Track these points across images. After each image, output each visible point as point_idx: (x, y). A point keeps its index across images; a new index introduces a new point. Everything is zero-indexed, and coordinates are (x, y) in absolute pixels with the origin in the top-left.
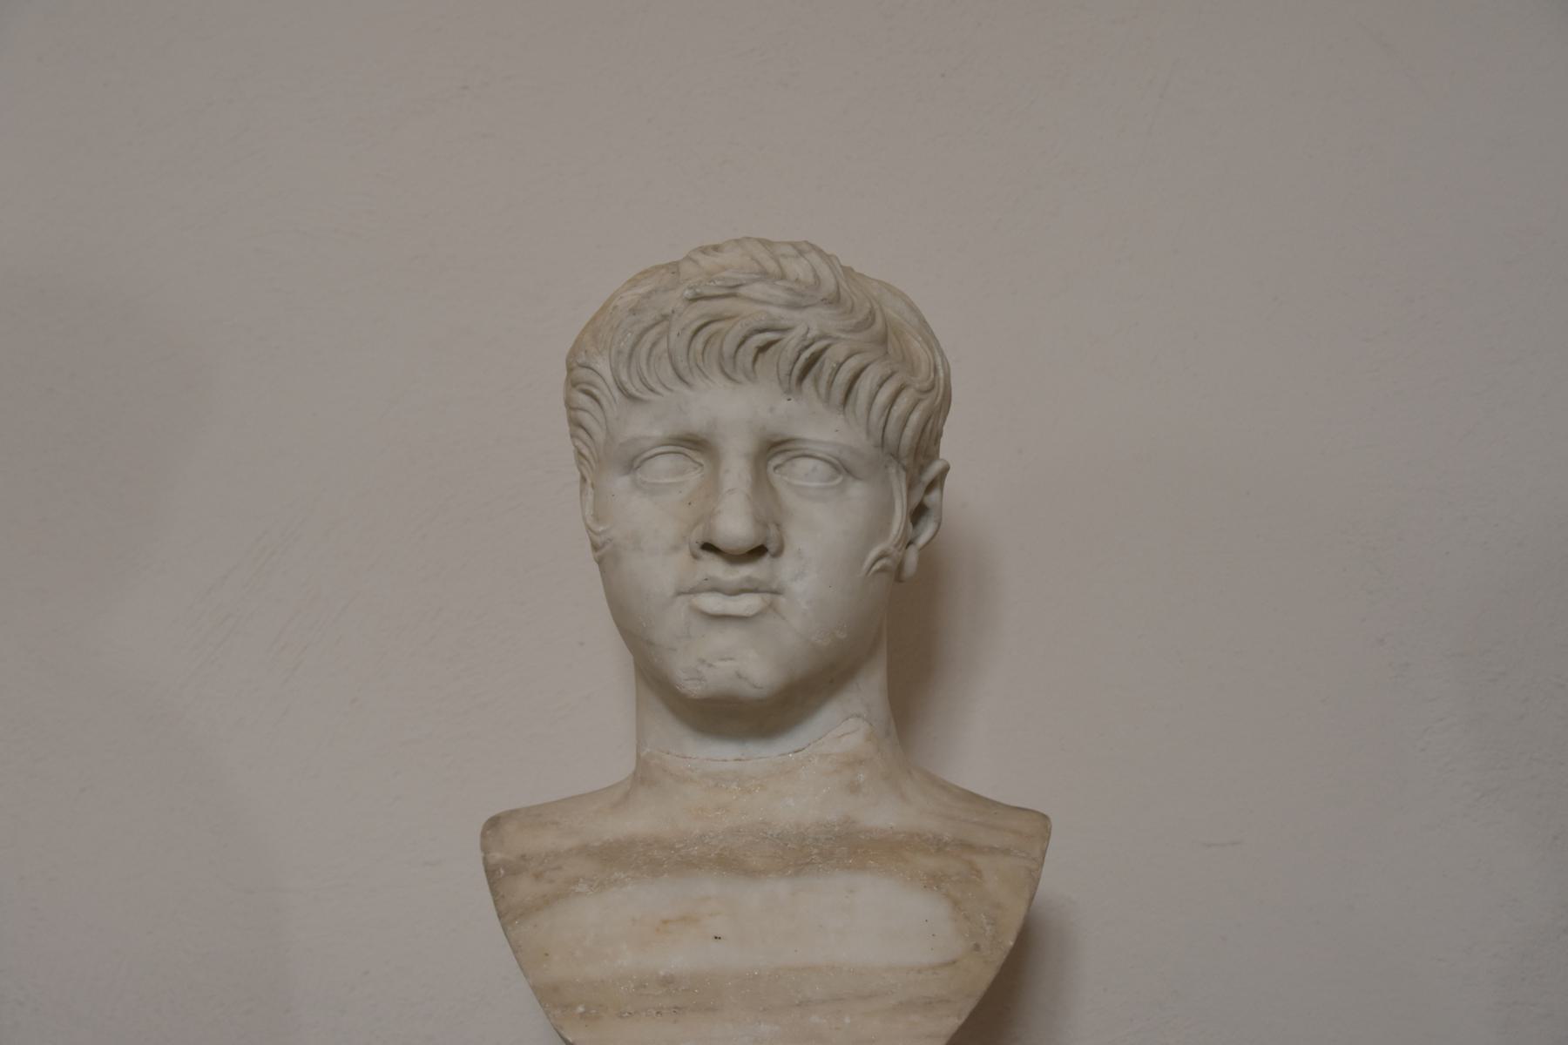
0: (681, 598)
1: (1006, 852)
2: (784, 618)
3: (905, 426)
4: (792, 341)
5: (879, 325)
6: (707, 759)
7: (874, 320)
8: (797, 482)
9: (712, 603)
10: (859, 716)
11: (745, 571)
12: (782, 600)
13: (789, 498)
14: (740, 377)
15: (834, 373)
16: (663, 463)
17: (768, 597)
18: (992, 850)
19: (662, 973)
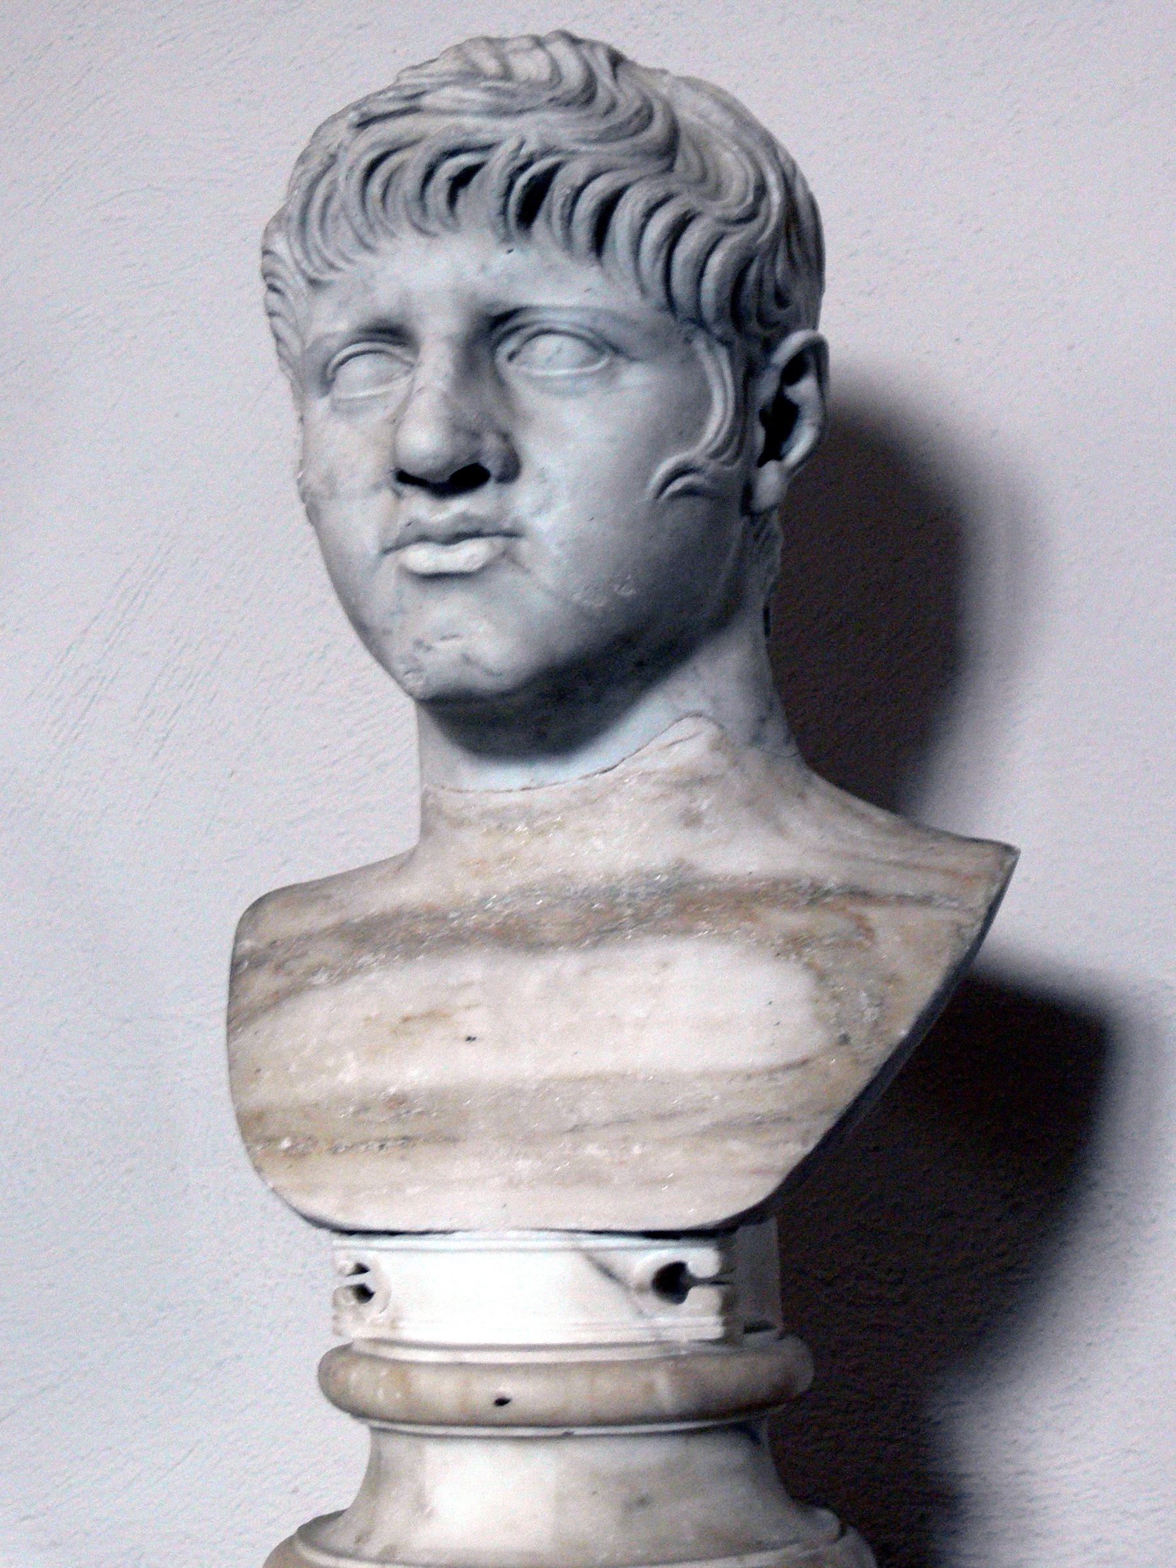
0: (390, 557)
1: (926, 900)
2: (528, 571)
3: (701, 274)
4: (498, 165)
5: (658, 129)
6: (487, 791)
7: (650, 117)
8: (539, 373)
9: (423, 558)
10: (698, 715)
11: (459, 506)
12: (524, 546)
13: (527, 396)
14: (434, 227)
15: (569, 203)
16: (360, 369)
17: (499, 542)
18: (902, 899)
19: (392, 1090)
